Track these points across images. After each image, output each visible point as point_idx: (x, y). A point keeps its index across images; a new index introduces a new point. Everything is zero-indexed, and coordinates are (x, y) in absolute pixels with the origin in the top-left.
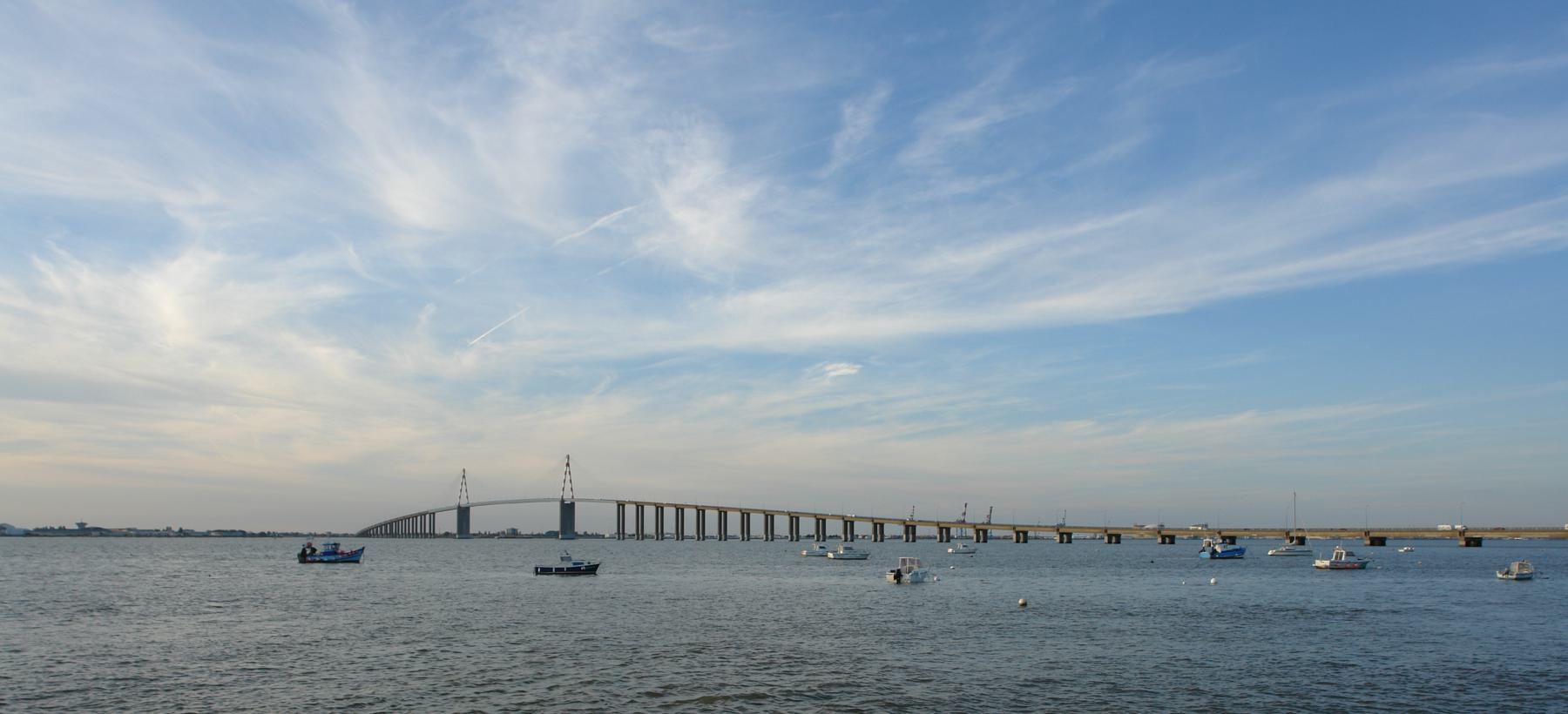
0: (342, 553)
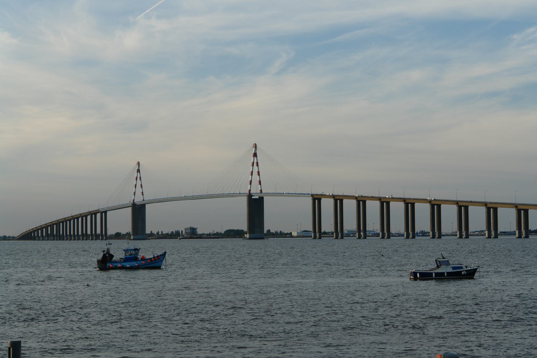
0: (143, 259)
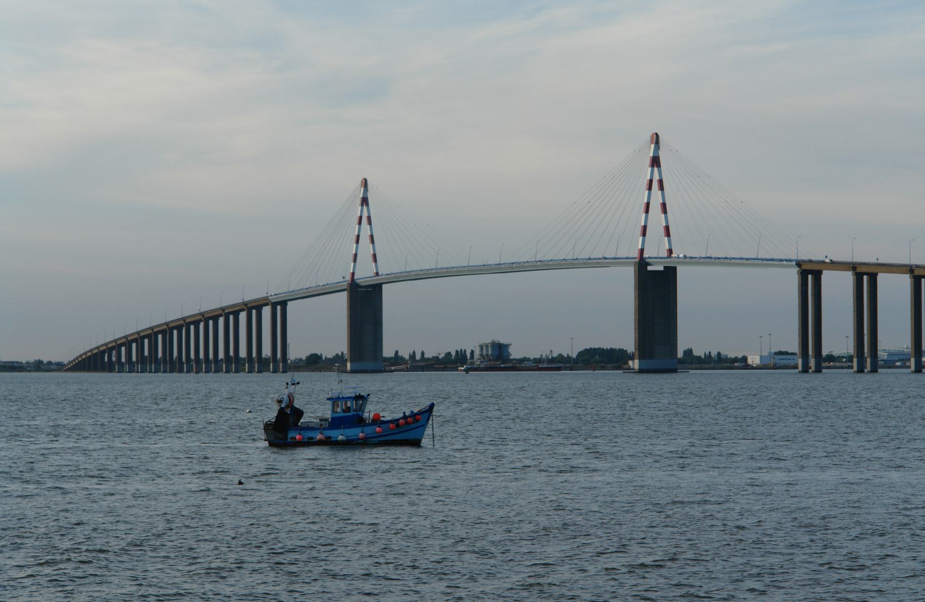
0: (377, 421)
